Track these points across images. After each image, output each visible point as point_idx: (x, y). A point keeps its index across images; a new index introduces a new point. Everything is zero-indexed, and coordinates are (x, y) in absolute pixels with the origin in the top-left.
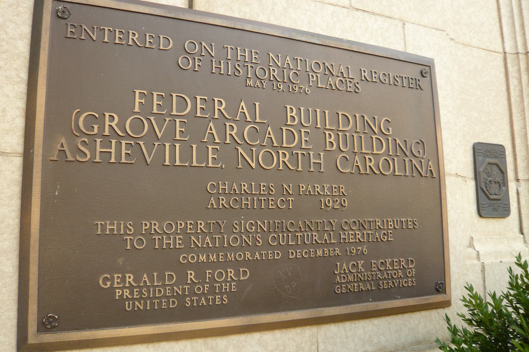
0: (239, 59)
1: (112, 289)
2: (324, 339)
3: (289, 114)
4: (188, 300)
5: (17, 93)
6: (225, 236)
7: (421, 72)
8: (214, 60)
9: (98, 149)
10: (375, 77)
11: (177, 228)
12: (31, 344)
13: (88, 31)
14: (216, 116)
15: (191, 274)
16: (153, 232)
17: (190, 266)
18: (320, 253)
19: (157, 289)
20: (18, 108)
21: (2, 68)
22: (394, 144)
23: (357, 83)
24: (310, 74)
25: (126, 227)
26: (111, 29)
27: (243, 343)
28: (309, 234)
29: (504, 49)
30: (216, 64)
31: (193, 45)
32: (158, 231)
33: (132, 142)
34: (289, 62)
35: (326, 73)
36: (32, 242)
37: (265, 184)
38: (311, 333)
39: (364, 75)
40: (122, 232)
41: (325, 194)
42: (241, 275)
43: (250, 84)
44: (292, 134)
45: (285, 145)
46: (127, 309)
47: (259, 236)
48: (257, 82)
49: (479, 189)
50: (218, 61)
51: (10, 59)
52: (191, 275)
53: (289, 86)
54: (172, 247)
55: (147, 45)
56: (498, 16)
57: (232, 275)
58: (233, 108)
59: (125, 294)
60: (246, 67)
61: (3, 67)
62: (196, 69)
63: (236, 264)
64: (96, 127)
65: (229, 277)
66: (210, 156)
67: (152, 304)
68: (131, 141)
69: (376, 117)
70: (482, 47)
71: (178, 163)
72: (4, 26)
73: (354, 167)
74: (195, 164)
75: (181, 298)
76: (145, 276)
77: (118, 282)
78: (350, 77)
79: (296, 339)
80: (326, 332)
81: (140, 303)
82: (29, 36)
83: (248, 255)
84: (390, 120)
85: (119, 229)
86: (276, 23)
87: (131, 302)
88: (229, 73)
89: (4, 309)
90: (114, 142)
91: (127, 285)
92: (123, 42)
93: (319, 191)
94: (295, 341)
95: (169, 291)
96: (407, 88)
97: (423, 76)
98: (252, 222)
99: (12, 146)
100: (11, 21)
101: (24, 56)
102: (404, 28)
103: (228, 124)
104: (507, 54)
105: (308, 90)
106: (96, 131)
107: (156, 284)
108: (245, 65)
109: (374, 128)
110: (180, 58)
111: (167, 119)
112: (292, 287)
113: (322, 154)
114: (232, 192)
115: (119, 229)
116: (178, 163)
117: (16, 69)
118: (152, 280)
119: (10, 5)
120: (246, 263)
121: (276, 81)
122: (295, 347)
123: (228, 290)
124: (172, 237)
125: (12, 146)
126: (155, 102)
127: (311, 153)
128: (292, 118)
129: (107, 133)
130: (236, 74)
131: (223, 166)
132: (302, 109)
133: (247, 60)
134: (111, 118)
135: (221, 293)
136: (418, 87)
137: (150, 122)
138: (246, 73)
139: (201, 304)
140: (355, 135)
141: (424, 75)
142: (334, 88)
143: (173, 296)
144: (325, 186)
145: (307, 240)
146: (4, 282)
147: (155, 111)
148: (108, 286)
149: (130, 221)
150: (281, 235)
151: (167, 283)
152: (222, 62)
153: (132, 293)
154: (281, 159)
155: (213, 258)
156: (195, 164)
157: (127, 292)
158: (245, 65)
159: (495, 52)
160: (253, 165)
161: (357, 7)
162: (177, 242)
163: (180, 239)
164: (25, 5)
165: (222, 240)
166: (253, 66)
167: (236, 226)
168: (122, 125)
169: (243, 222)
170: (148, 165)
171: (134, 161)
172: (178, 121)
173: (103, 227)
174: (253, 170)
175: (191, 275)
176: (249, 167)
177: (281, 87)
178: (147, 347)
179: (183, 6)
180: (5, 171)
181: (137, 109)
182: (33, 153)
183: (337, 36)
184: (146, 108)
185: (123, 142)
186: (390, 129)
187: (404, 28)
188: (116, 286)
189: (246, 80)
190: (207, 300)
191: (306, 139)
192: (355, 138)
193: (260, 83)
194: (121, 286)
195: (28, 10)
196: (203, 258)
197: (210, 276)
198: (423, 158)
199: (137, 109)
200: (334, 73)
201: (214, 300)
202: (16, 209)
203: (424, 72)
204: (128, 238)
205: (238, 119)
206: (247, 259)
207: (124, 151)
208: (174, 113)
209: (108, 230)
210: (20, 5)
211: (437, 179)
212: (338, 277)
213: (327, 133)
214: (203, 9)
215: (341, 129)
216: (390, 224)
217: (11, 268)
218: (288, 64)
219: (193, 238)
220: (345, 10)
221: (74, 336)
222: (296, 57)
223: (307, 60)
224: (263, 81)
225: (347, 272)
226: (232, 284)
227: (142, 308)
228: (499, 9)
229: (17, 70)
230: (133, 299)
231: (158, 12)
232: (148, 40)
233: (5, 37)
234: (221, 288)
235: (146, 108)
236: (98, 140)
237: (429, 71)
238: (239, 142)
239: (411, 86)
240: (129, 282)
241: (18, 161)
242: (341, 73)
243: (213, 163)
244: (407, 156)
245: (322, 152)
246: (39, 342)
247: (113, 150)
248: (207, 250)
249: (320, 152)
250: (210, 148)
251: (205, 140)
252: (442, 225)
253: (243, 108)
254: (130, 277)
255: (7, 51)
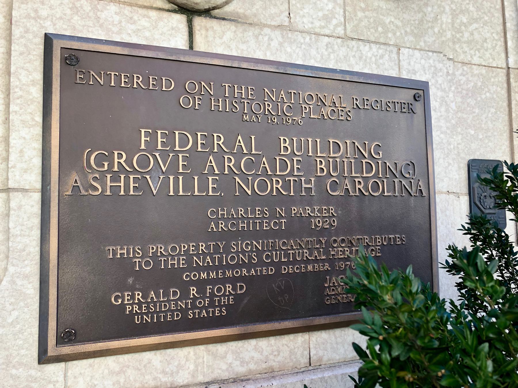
0: (236, 96)
1: (123, 306)
2: (316, 345)
3: (282, 145)
4: (191, 313)
5: (33, 136)
6: (224, 256)
7: (414, 96)
8: (213, 99)
9: (109, 184)
10: (367, 105)
11: (180, 249)
12: (50, 356)
13: (96, 76)
14: (216, 150)
15: (193, 290)
16: (159, 255)
17: (192, 283)
18: (310, 268)
19: (163, 304)
20: (35, 149)
21: (18, 112)
22: (384, 167)
23: (349, 111)
24: (303, 106)
25: (134, 251)
26: (117, 74)
27: (241, 349)
28: (301, 251)
29: (507, 64)
30: (214, 102)
31: (194, 85)
32: (164, 253)
33: (139, 177)
34: (283, 96)
35: (319, 104)
36: (51, 267)
37: (260, 209)
38: (303, 340)
39: (356, 103)
40: (131, 256)
41: (316, 215)
42: (238, 290)
43: (246, 119)
44: (286, 163)
45: (278, 173)
46: (137, 322)
47: (254, 255)
48: (253, 117)
49: (472, 203)
50: (216, 99)
51: (24, 104)
52: (193, 291)
53: (283, 119)
54: (176, 267)
55: (151, 88)
56: (503, 31)
57: (230, 289)
58: (230, 143)
59: (135, 309)
60: (243, 103)
61: (18, 111)
62: (197, 108)
63: (233, 281)
64: (106, 164)
65: (227, 291)
66: (211, 186)
67: (158, 318)
68: (138, 175)
69: (367, 143)
70: (483, 64)
71: (181, 193)
72: (17, 73)
73: (344, 190)
74: (196, 193)
75: (184, 311)
76: (152, 293)
77: (128, 299)
78: (343, 105)
79: (289, 345)
80: (317, 338)
81: (148, 317)
82: (41, 82)
83: (245, 272)
84: (380, 145)
85: (128, 253)
86: (272, 59)
87: (140, 316)
88: (227, 110)
89: (27, 326)
90: (122, 177)
91: (136, 301)
92: (128, 85)
93: (310, 213)
94: (288, 346)
95: (174, 306)
96: (399, 113)
97: (416, 100)
98: (248, 242)
99: (30, 183)
100: (23, 68)
101: (37, 101)
102: (398, 53)
103: (226, 157)
104: (510, 69)
105: (301, 122)
106: (106, 168)
107: (162, 299)
108: (242, 101)
109: (364, 153)
110: (182, 98)
111: (171, 155)
112: (285, 300)
113: (313, 179)
114: (230, 217)
115: (128, 253)
116: (181, 193)
117: (31, 113)
118: (158, 296)
119: (21, 54)
120: (242, 279)
121: (270, 114)
122: (288, 352)
123: (226, 303)
124: (176, 258)
125: (30, 183)
126: (160, 140)
127: (303, 179)
128: (285, 148)
129: (116, 169)
130: (233, 110)
131: (222, 194)
132: (295, 139)
133: (243, 97)
134: (120, 156)
135: (220, 306)
136: (410, 111)
137: (155, 157)
138: (243, 109)
139: (202, 316)
140: (345, 160)
141: (417, 99)
142: (325, 118)
143: (177, 310)
144: (315, 208)
145: (298, 256)
146: (26, 302)
147: (160, 147)
148: (120, 302)
149: (138, 245)
150: (274, 253)
151: (172, 298)
152: (220, 100)
153: (140, 308)
154: (275, 186)
155: (213, 275)
156: (196, 193)
157: (136, 308)
158: (242, 101)
159: (498, 68)
160: (249, 192)
161: (352, 36)
162: (181, 262)
163: (183, 259)
164: (35, 53)
165: (220, 260)
166: (249, 102)
167: (233, 246)
168: (129, 162)
169: (240, 242)
170: (154, 196)
171: (141, 193)
172: (180, 155)
173: (115, 253)
174: (249, 197)
175: (193, 291)
176: (245, 194)
177: (276, 120)
178: (155, 354)
179: (184, 48)
180: (24, 205)
181: (143, 147)
182: (50, 189)
183: (331, 67)
184: (152, 146)
185: (132, 177)
186: (381, 153)
187: (398, 53)
188: (126, 302)
189: (243, 115)
190: (208, 313)
191: (298, 166)
192: (345, 163)
193: (256, 117)
194: (131, 302)
195: (38, 58)
196: (204, 276)
197: (210, 291)
198: (413, 178)
199: (143, 147)
200: (326, 104)
201: (214, 312)
202: (36, 239)
203: (417, 96)
204: (137, 260)
205: (235, 151)
206: (243, 275)
207: (132, 185)
208: (177, 148)
209: (119, 254)
210: (31, 53)
211: (427, 198)
212: (328, 290)
213: (318, 160)
214: (202, 49)
215: (332, 155)
216: (378, 240)
217: (32, 290)
218: (282, 98)
219: (195, 258)
220: (339, 41)
221: (89, 348)
222: (290, 90)
223: (301, 93)
224: (258, 116)
225: (336, 284)
226: (231, 297)
227: (149, 321)
228: (504, 23)
229: (32, 114)
230: (142, 314)
231: (161, 55)
232: (151, 82)
233: (18, 83)
234: (219, 301)
235: (152, 146)
236: (109, 176)
237: (422, 95)
238: (236, 172)
239: (404, 110)
240: (138, 298)
241: (37, 196)
242: (334, 103)
243: (212, 192)
244: (397, 178)
245: (313, 177)
246: (58, 354)
247: (122, 184)
248: (208, 269)
249: (311, 177)
250: (210, 178)
251: (206, 172)
252: (431, 240)
253: (240, 142)
254: (138, 295)
255: (21, 97)
